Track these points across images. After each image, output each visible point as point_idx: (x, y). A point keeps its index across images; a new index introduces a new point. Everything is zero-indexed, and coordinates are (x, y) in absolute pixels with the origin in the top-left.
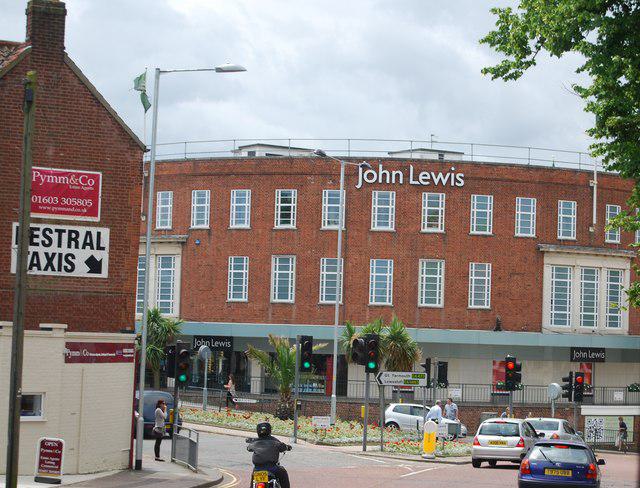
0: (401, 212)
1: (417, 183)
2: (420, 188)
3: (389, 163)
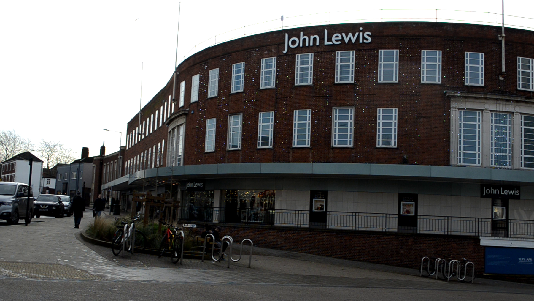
0: (359, 71)
1: (330, 43)
2: (334, 48)
3: (308, 31)
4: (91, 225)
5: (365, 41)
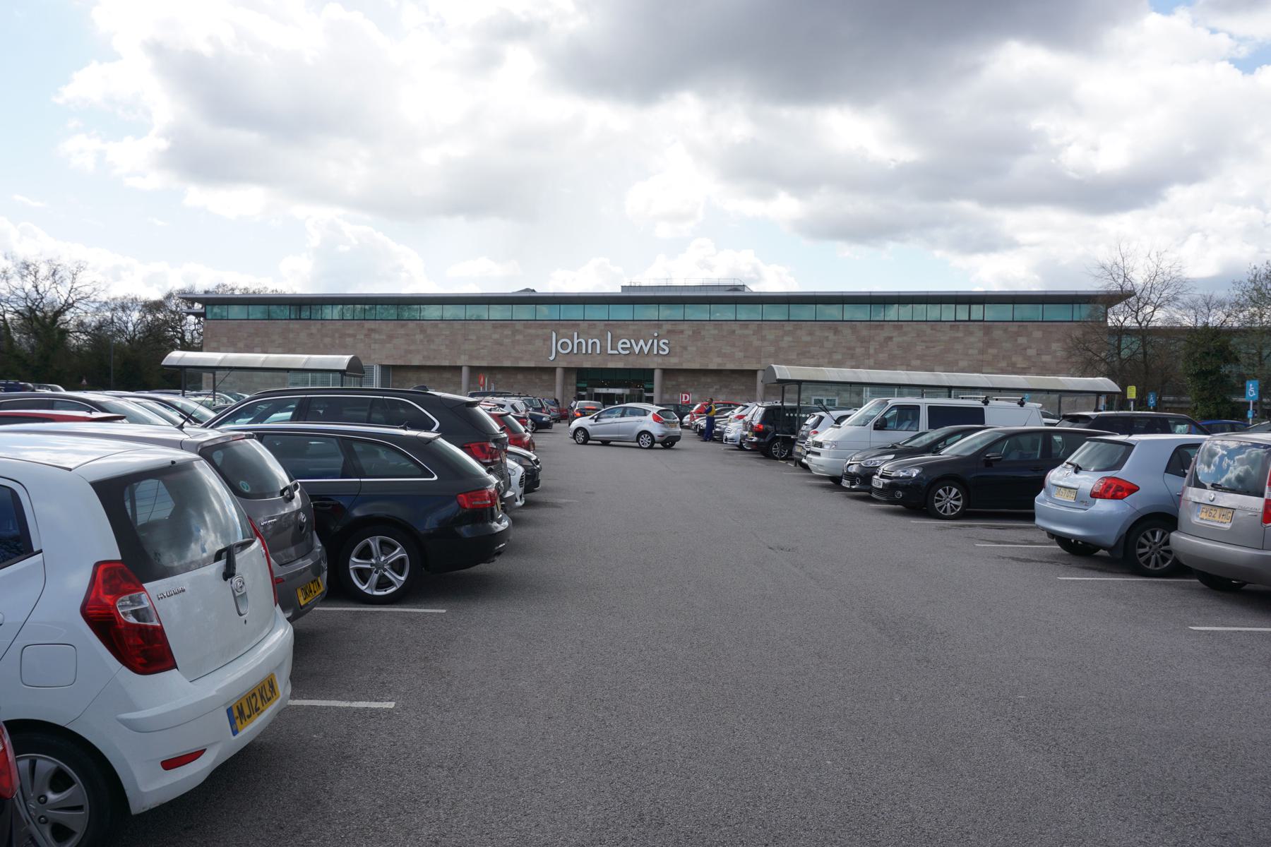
4: (105, 320)
5: (661, 352)
